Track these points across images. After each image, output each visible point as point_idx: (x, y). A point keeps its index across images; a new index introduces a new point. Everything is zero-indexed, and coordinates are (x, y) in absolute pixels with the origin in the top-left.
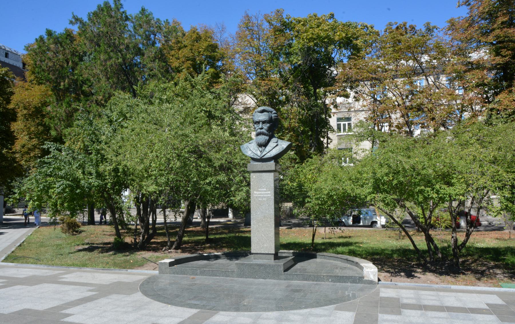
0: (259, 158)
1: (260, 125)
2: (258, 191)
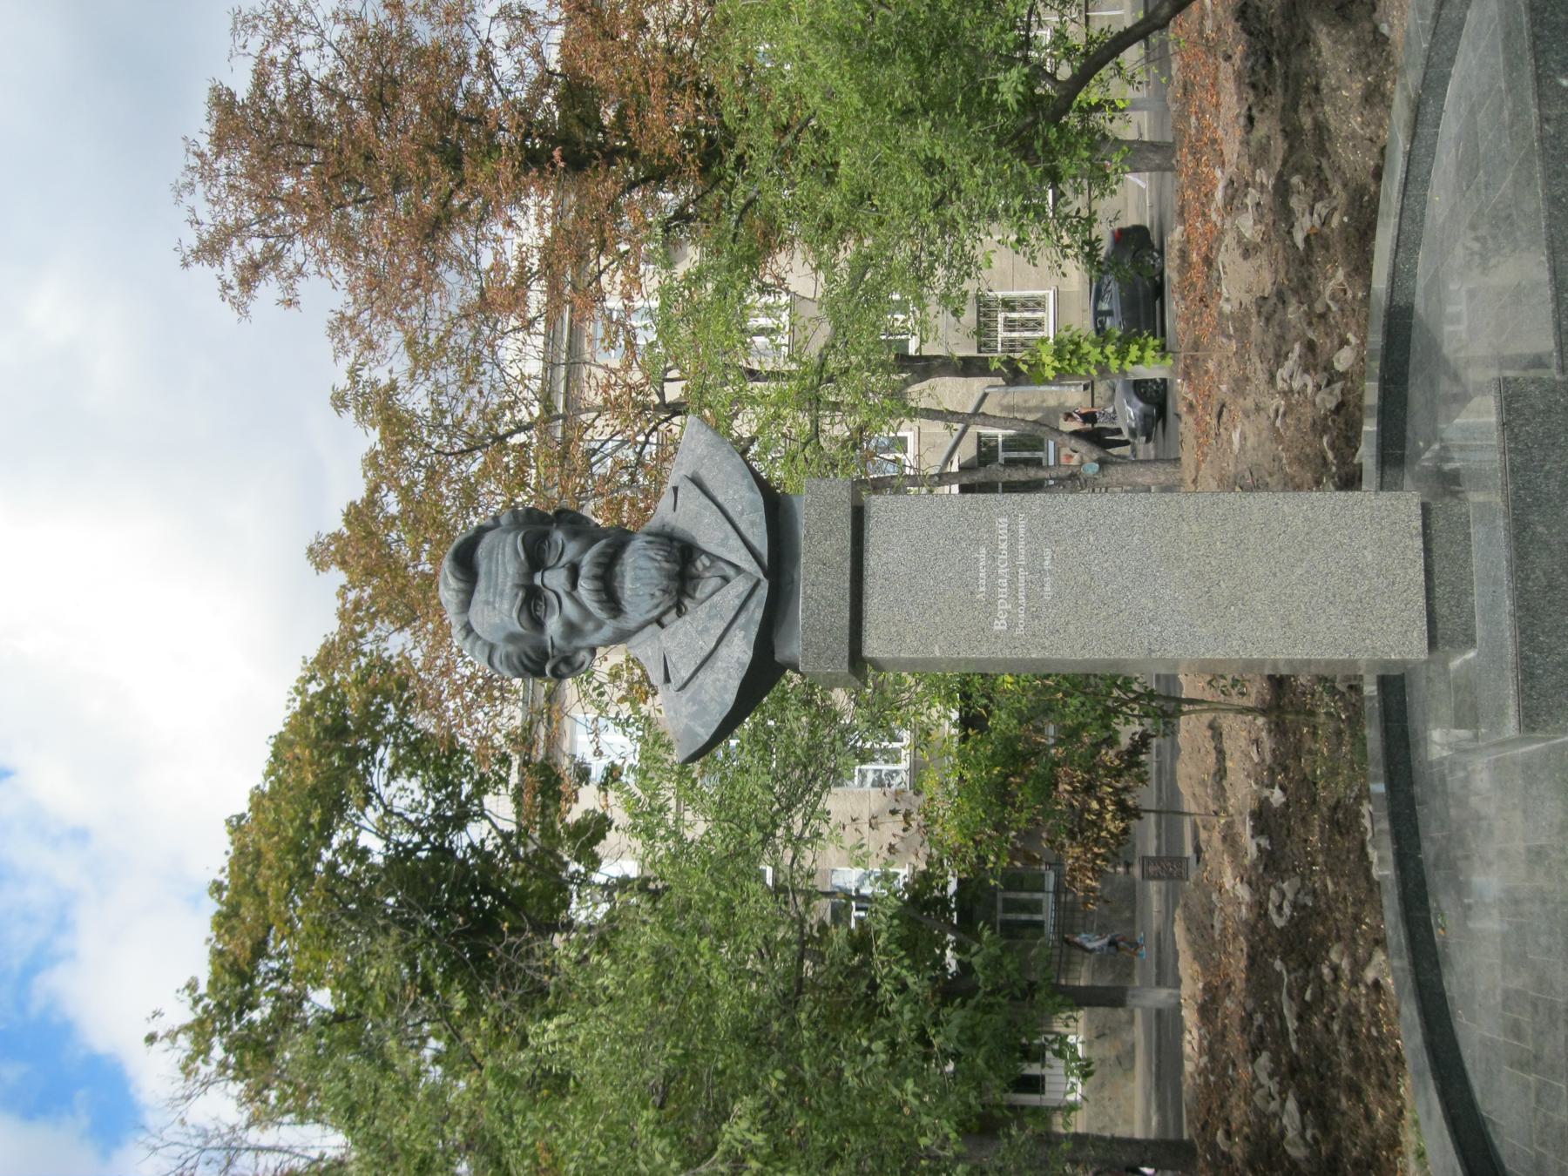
0: (763, 591)
1: (555, 579)
2: (991, 601)
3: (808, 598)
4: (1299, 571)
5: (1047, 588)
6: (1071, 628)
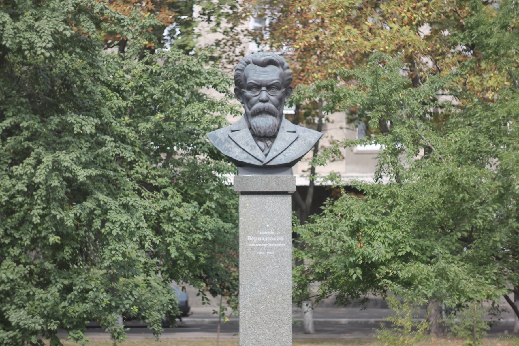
0: (258, 163)
1: (264, 95)
2: (257, 235)
3: (257, 178)
4: (267, 331)
5: (261, 253)
6: (248, 260)
